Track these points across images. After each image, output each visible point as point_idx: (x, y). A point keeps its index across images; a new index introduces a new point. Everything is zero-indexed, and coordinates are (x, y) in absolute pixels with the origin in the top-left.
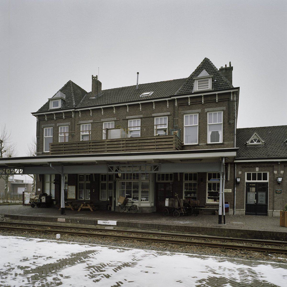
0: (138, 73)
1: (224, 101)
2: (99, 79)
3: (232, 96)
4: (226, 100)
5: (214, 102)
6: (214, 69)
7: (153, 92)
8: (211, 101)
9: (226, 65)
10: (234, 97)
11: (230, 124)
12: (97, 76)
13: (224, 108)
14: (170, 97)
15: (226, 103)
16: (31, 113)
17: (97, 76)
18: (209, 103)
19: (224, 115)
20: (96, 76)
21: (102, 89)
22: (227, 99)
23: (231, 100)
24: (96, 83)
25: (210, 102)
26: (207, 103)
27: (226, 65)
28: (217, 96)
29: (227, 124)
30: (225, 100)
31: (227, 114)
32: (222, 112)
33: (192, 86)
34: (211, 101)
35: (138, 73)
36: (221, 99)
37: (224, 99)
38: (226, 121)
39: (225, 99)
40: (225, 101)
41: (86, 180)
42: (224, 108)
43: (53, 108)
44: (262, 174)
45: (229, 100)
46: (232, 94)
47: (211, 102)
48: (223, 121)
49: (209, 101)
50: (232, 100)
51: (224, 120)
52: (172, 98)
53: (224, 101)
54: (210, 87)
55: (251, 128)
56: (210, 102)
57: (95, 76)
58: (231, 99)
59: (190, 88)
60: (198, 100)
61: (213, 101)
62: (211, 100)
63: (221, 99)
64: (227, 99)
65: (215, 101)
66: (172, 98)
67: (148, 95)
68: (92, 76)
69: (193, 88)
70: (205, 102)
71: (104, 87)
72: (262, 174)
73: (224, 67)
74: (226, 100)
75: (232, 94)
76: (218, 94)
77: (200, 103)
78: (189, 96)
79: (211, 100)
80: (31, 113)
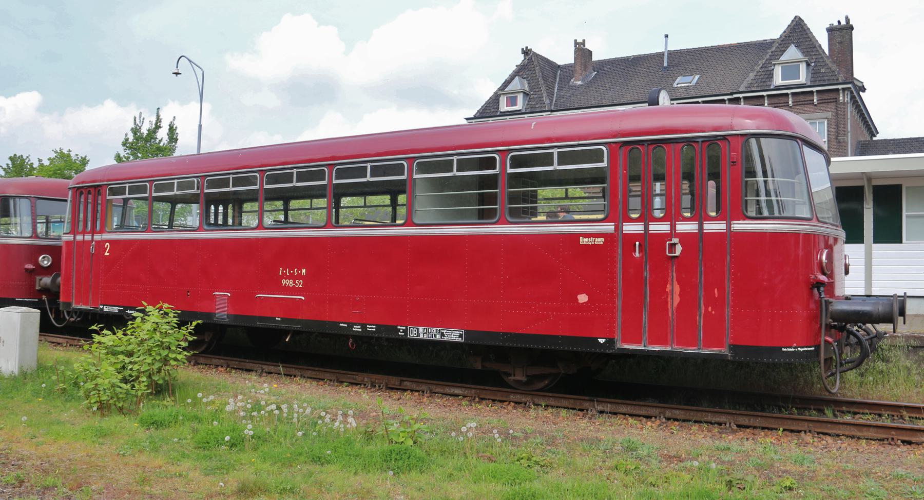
0: (667, 36)
1: (828, 102)
2: (588, 46)
3: (841, 95)
4: (832, 100)
5: (810, 104)
6: (811, 40)
7: (699, 76)
8: (806, 103)
9: (839, 22)
10: (846, 96)
11: (839, 142)
12: (584, 41)
13: (829, 115)
14: (732, 94)
15: (832, 105)
16: (465, 119)
17: (584, 41)
18: (802, 104)
19: (828, 126)
20: (582, 41)
21: (593, 60)
22: (833, 99)
23: (841, 101)
24: (582, 52)
25: (804, 103)
26: (798, 105)
27: (839, 22)
28: (815, 94)
29: (834, 143)
30: (829, 101)
31: (834, 126)
32: (824, 122)
33: (770, 74)
34: (806, 103)
35: (667, 36)
36: (822, 100)
37: (828, 99)
38: (833, 137)
39: (830, 99)
40: (831, 102)
41: (826, 299)
42: (829, 115)
43: (507, 108)
45: (836, 100)
46: (841, 92)
47: (805, 104)
48: (828, 137)
49: (802, 101)
50: (842, 101)
51: (828, 135)
52: (735, 96)
53: (828, 102)
54: (803, 78)
55: (891, 140)
56: (804, 103)
57: (580, 40)
58: (839, 100)
59: (768, 78)
60: (783, 100)
61: (809, 102)
62: (805, 101)
63: (822, 100)
64: (833, 99)
65: (811, 102)
66: (735, 96)
67: (689, 84)
68: (576, 41)
69: (772, 77)
70: (795, 104)
73: (836, 24)
74: (832, 100)
75: (841, 92)
76: (818, 92)
77: (811, 102)
78: (765, 94)
79: (805, 101)
80: (465, 119)
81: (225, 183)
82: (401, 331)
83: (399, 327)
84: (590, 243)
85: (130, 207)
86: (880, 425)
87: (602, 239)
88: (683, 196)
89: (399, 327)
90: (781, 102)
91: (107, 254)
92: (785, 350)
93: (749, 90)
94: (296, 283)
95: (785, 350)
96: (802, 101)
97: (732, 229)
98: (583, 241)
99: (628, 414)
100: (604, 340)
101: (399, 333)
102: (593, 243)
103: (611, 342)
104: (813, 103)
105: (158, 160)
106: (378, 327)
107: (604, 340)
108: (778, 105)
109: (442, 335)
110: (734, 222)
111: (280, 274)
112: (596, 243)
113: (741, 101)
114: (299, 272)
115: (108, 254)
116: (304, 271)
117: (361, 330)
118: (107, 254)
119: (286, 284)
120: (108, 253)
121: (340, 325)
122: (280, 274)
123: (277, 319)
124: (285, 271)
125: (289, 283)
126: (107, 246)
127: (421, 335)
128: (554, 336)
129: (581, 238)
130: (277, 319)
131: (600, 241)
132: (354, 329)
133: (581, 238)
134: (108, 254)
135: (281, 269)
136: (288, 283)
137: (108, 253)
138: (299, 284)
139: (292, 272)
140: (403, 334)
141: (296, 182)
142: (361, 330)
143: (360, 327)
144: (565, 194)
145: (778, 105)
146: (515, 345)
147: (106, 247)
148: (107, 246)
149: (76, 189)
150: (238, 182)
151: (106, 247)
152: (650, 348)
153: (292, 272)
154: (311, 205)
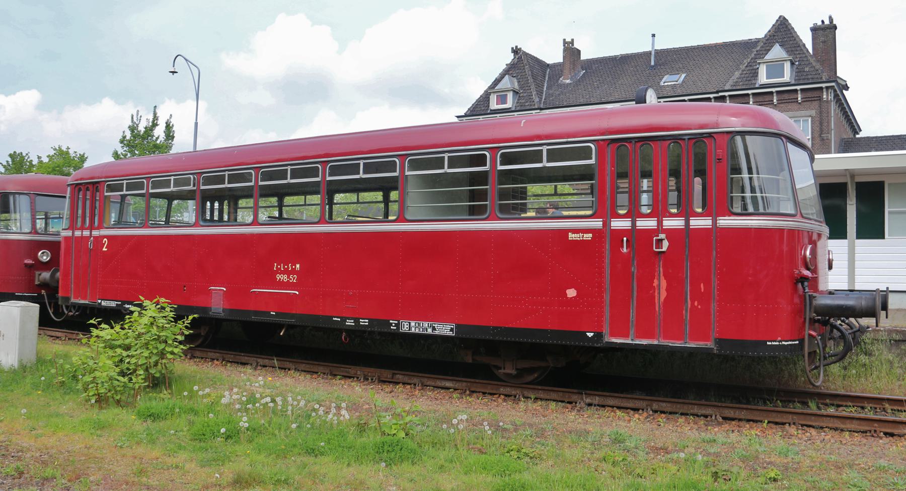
0: (654, 35)
1: (812, 100)
2: (576, 45)
3: (825, 93)
4: (816, 99)
5: (794, 102)
6: (795, 40)
7: (685, 74)
8: (790, 101)
9: (823, 22)
10: (830, 94)
11: (823, 140)
12: (573, 40)
13: (813, 113)
14: (717, 92)
15: (816, 103)
16: (456, 116)
17: (573, 40)
18: (787, 102)
19: (812, 124)
20: (570, 40)
22: (817, 97)
23: (824, 99)
24: (571, 51)
25: (788, 101)
26: (782, 103)
27: (823, 22)
28: (799, 92)
29: (818, 141)
30: (813, 99)
31: (818, 123)
32: (808, 120)
33: (755, 73)
34: (790, 101)
35: (654, 35)
36: (806, 98)
37: (812, 97)
38: (817, 135)
39: (814, 97)
40: (814, 100)
42: (813, 113)
43: (498, 106)
44: (172, 185)
45: (820, 99)
46: (824, 90)
47: (789, 102)
48: (812, 135)
49: (786, 100)
50: (825, 99)
51: (812, 132)
52: (721, 94)
53: (812, 100)
54: (787, 77)
55: (874, 137)
56: (788, 101)
57: (568, 40)
58: (823, 98)
59: (753, 76)
60: (767, 98)
61: (793, 100)
62: (789, 99)
63: (806, 98)
64: (817, 97)
65: (796, 100)
66: (721, 94)
67: (676, 83)
68: (564, 40)
69: (757, 76)
70: (780, 102)
71: (566, 41)
72: (172, 185)
73: (820, 23)
74: (816, 99)
75: (824, 90)
76: (802, 90)
77: (796, 100)
78: (750, 92)
79: (789, 99)
80: (456, 116)
81: (220, 180)
82: (393, 325)
83: (391, 321)
84: (579, 239)
85: (127, 203)
86: (863, 418)
87: (591, 235)
88: (670, 193)
89: (391, 321)
90: (766, 100)
91: (105, 249)
92: (770, 343)
93: (734, 88)
94: (291, 277)
95: (770, 343)
96: (786, 100)
97: (718, 225)
98: (571, 236)
99: (616, 407)
100: (592, 334)
101: (392, 327)
102: (581, 239)
103: (599, 336)
104: (797, 102)
105: (155, 157)
106: (370, 321)
107: (592, 334)
108: (763, 103)
109: (434, 329)
110: (720, 218)
111: (275, 269)
112: (584, 239)
113: (726, 99)
114: (294, 267)
115: (106, 250)
116: (298, 266)
117: (354, 324)
118: (105, 249)
119: (280, 279)
120: (106, 248)
121: (334, 319)
122: (275, 269)
123: (272, 313)
124: (279, 267)
125: (283, 278)
126: (105, 241)
127: (413, 329)
128: (543, 330)
129: (570, 233)
130: (272, 313)
131: (588, 236)
132: (347, 324)
133: (570, 233)
134: (106, 250)
135: (275, 264)
136: (282, 278)
137: (106, 248)
138: (294, 279)
139: (286, 267)
140: (395, 328)
141: (291, 179)
142: (354, 324)
143: (353, 321)
144: (554, 191)
145: (763, 103)
146: (505, 338)
147: (104, 242)
148: (105, 241)
149: (74, 185)
150: (233, 179)
151: (104, 242)
152: (637, 342)
153: (286, 267)
154: (305, 201)
